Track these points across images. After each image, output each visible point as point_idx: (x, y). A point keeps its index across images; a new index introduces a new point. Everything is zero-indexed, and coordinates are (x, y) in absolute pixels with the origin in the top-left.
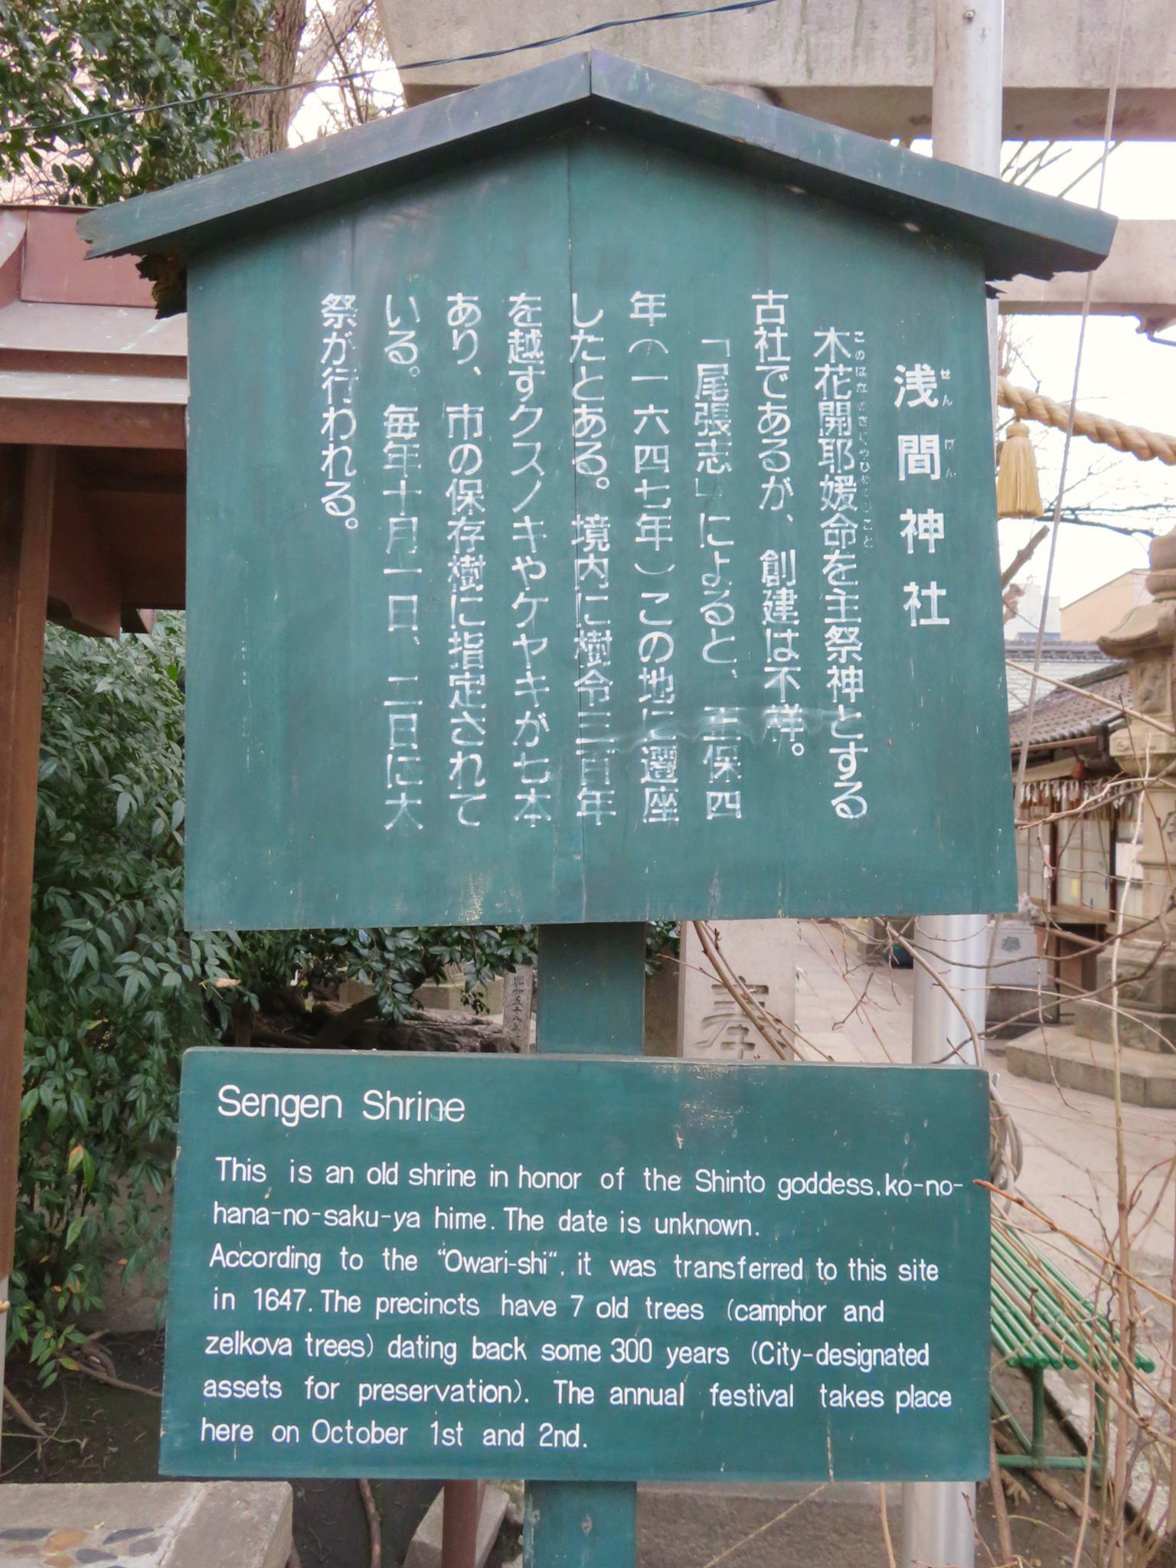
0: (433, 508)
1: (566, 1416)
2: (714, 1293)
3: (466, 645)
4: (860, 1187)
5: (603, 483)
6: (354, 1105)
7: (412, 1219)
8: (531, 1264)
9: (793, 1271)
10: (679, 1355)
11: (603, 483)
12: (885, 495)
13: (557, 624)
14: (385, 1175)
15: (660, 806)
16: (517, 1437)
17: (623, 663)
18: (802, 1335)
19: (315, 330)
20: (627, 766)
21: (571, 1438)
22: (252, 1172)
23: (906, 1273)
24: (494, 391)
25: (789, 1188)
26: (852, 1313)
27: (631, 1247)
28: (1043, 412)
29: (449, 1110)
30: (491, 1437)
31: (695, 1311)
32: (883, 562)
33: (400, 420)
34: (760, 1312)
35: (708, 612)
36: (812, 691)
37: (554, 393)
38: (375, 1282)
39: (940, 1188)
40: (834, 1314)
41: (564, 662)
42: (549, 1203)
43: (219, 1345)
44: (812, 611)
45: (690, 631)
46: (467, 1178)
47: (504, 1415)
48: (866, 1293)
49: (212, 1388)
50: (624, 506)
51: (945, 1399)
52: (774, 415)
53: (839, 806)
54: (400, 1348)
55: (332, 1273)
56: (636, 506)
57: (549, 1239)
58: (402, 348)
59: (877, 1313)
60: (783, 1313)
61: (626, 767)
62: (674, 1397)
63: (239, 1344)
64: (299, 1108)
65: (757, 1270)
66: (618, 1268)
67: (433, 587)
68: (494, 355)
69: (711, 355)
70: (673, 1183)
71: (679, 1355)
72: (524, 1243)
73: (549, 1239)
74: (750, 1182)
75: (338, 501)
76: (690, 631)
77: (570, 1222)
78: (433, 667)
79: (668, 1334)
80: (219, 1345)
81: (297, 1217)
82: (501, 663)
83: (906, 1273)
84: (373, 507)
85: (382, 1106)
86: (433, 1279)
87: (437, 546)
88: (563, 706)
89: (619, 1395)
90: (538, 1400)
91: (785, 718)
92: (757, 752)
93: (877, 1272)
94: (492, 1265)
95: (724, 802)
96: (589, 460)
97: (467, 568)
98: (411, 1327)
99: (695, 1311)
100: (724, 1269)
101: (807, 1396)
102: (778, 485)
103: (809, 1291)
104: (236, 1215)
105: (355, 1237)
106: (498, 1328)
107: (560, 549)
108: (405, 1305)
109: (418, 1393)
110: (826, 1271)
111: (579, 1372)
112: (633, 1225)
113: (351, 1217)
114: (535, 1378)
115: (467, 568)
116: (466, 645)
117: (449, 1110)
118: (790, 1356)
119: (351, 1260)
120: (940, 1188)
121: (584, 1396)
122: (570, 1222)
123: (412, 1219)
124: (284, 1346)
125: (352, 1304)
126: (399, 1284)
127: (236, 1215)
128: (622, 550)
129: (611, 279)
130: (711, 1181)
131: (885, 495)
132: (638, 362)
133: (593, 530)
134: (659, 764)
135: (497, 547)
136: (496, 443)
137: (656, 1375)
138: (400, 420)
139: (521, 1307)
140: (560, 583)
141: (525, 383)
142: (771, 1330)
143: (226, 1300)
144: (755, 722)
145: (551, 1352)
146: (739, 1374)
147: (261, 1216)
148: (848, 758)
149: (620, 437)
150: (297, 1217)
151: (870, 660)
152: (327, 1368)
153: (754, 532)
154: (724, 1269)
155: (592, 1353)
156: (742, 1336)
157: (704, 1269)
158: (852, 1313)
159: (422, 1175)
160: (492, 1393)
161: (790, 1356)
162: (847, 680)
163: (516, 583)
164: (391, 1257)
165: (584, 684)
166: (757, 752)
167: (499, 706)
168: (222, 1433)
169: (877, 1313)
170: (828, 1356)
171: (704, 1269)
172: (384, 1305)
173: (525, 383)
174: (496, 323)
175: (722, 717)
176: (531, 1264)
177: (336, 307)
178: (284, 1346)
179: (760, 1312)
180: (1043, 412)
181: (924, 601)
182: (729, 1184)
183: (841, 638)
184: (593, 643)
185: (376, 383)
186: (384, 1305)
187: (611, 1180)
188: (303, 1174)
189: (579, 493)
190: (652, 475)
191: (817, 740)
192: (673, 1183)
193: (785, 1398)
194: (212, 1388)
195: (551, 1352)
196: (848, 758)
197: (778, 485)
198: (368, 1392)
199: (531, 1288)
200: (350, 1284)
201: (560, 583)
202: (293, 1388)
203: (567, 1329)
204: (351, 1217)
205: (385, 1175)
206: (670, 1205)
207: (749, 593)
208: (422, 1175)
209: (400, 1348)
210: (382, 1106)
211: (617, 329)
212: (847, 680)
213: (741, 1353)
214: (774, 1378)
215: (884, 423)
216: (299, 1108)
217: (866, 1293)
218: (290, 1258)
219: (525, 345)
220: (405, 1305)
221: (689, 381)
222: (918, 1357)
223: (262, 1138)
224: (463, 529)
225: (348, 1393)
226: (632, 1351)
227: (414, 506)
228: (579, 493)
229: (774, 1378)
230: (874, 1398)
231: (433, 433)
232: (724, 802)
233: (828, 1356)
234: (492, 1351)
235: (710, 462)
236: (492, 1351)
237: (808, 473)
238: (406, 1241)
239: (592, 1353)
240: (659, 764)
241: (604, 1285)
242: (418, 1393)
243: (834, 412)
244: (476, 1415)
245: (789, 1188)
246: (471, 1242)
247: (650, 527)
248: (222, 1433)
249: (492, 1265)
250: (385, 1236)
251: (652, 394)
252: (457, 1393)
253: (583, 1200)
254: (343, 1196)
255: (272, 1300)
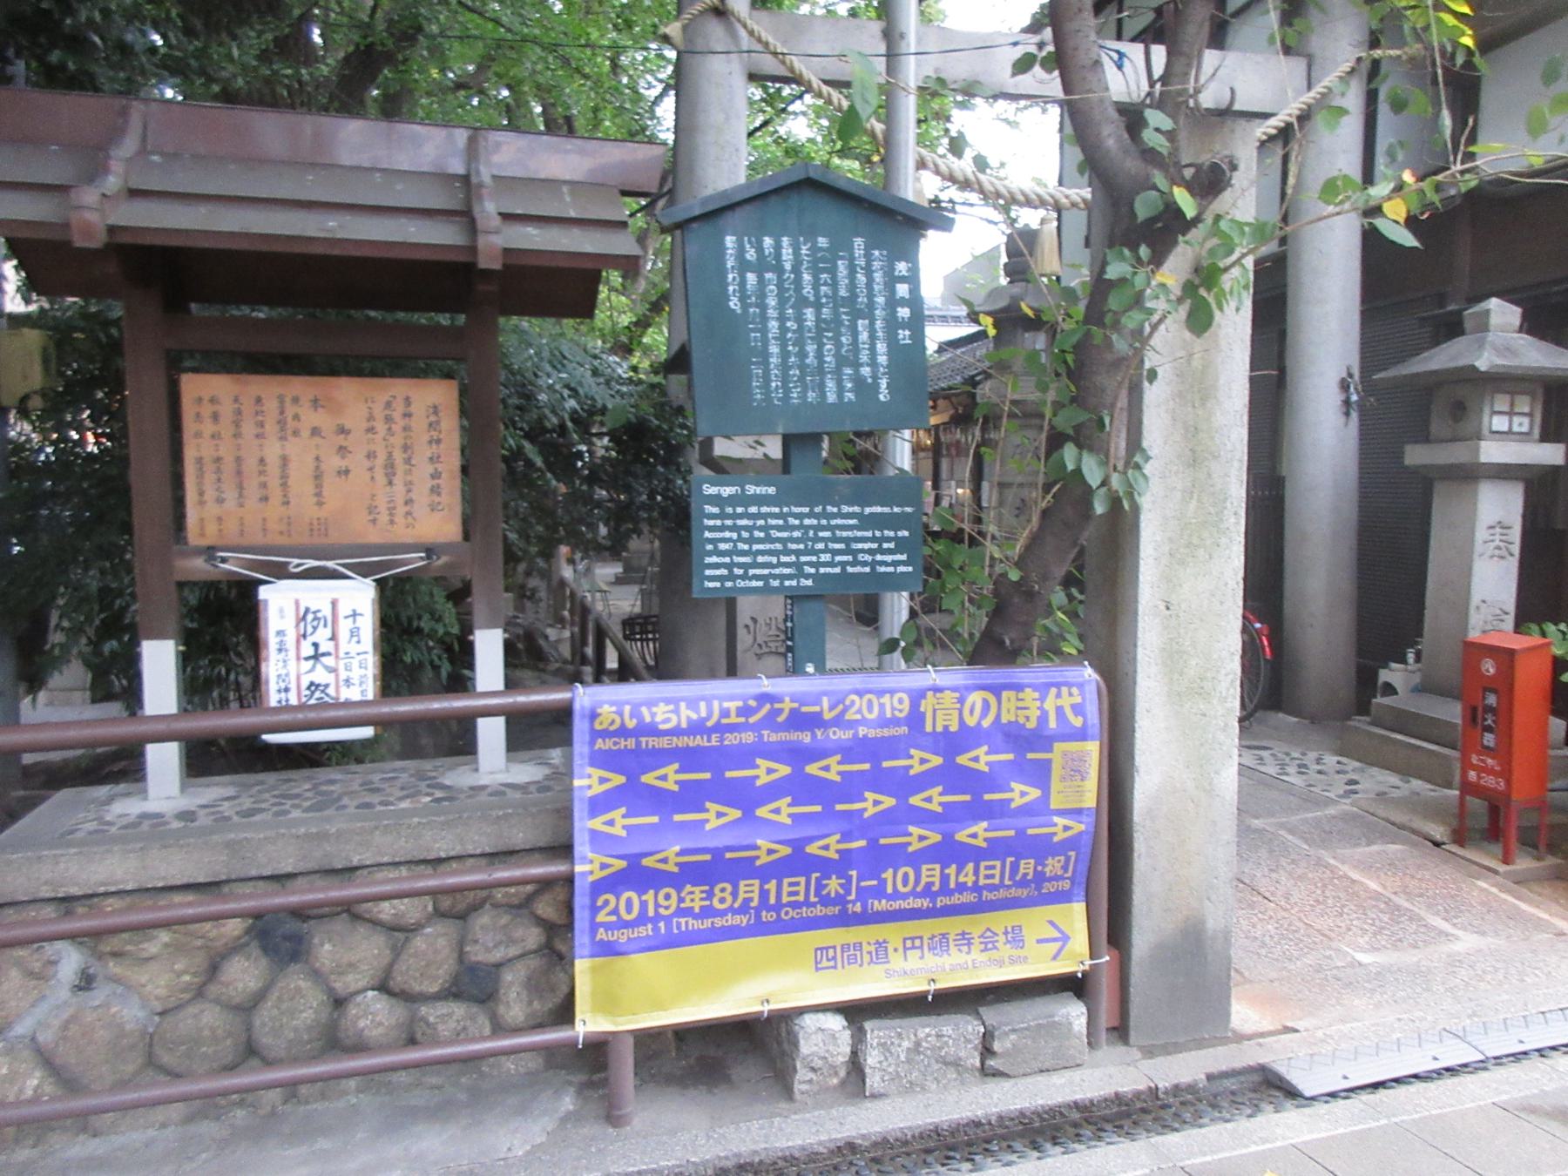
0: (763, 307)
1: (807, 577)
2: (847, 541)
3: (774, 349)
4: (886, 510)
5: (812, 299)
6: (743, 490)
7: (761, 522)
8: (796, 534)
9: (869, 534)
10: (838, 558)
11: (812, 299)
12: (893, 303)
13: (800, 342)
14: (753, 510)
15: (831, 397)
16: (794, 583)
17: (820, 355)
18: (871, 552)
19: (723, 248)
20: (822, 386)
21: (809, 583)
22: (715, 510)
23: (900, 534)
24: (779, 269)
25: (868, 510)
26: (885, 545)
27: (824, 528)
28: (1021, 198)
29: (771, 490)
30: (787, 583)
31: (842, 546)
32: (893, 324)
33: (751, 278)
34: (860, 546)
35: (844, 339)
36: (873, 363)
37: (796, 269)
38: (752, 540)
39: (909, 510)
40: (746, 572)
41: (802, 355)
42: (800, 516)
43: (708, 560)
44: (873, 337)
45: (838, 345)
46: (777, 510)
47: (789, 577)
48: (889, 540)
49: (708, 572)
50: (818, 306)
51: (911, 569)
52: (861, 278)
53: (881, 397)
54: (760, 559)
55: (740, 539)
56: (822, 305)
57: (801, 527)
58: (751, 255)
59: (892, 545)
60: (866, 546)
61: (821, 387)
62: (837, 570)
63: (714, 559)
64: (727, 491)
65: (859, 534)
66: (821, 534)
67: (764, 331)
68: (778, 255)
69: (842, 258)
70: (835, 510)
71: (838, 558)
72: (794, 528)
73: (801, 527)
74: (857, 509)
75: (734, 304)
76: (838, 345)
77: (807, 522)
78: (765, 355)
79: (835, 552)
80: (708, 560)
81: (729, 522)
82: (785, 354)
83: (900, 534)
84: (745, 306)
85: (752, 489)
86: (769, 539)
87: (764, 318)
88: (802, 367)
89: (822, 570)
90: (801, 574)
91: (866, 371)
92: (859, 381)
93: (892, 534)
94: (785, 535)
95: (849, 396)
96: (807, 290)
97: (773, 325)
98: (763, 553)
99: (842, 546)
100: (850, 534)
101: (873, 569)
102: (862, 299)
103: (873, 539)
104: (711, 523)
105: (746, 528)
106: (788, 552)
107: (800, 319)
108: (761, 547)
109: (766, 572)
110: (878, 534)
111: (810, 564)
112: (824, 522)
113: (744, 522)
114: (798, 566)
115: (773, 325)
116: (774, 349)
117: (771, 490)
118: (868, 558)
119: (745, 535)
120: (909, 510)
121: (813, 571)
122: (807, 522)
123: (761, 522)
124: (727, 560)
125: (746, 547)
126: (760, 541)
127: (711, 523)
128: (818, 320)
129: (811, 235)
130: (846, 509)
131: (893, 303)
132: (823, 260)
133: (809, 313)
134: (830, 385)
135: (782, 319)
136: (780, 285)
137: (831, 564)
138: (751, 278)
139: (794, 546)
140: (801, 328)
141: (788, 266)
142: (862, 551)
143: (710, 547)
144: (857, 371)
145: (803, 559)
146: (855, 563)
147: (719, 523)
148: (883, 383)
149: (816, 285)
150: (729, 522)
151: (890, 354)
152: (740, 565)
153: (856, 315)
154: (850, 534)
155: (814, 559)
156: (855, 553)
157: (845, 534)
158: (885, 545)
159: (764, 509)
160: (787, 571)
161: (868, 558)
162: (882, 359)
163: (788, 330)
164: (757, 534)
165: (808, 361)
166: (859, 381)
167: (785, 367)
168: (711, 585)
169: (892, 545)
170: (879, 557)
171: (845, 534)
172: (755, 547)
173: (788, 266)
174: (778, 247)
175: (848, 371)
176: (796, 534)
177: (730, 241)
178: (727, 560)
179: (860, 546)
180: (1021, 198)
181: (904, 335)
182: (851, 510)
183: (881, 347)
184: (811, 348)
185: (743, 266)
186: (755, 547)
187: (818, 509)
188: (729, 510)
189: (802, 302)
190: (826, 296)
191: (875, 377)
192: (835, 510)
193: (867, 569)
194: (708, 572)
195: (803, 559)
196: (883, 383)
197: (862, 299)
198: (752, 572)
199: (797, 541)
200: (745, 541)
201: (801, 328)
202: (731, 571)
203: (806, 552)
204: (744, 522)
205: (753, 510)
206: (834, 516)
207: (855, 333)
208: (764, 509)
209: (760, 559)
210: (752, 489)
211: (814, 249)
212: (882, 359)
213: (855, 558)
214: (865, 564)
215: (892, 280)
216: (727, 491)
217: (889, 540)
218: (727, 534)
219: (787, 253)
220: (761, 547)
221: (835, 266)
222: (904, 557)
223: (717, 500)
224: (772, 313)
225: (746, 572)
226: (825, 557)
227: (757, 306)
228: (802, 302)
229: (865, 564)
230: (891, 569)
231: (761, 282)
232: (849, 396)
233: (879, 557)
234: (784, 559)
235: (843, 293)
236: (784, 559)
237: (871, 296)
238: (760, 529)
239: (814, 559)
240: (830, 385)
241: (817, 539)
242: (766, 572)
243: (878, 276)
244: (783, 577)
245: (868, 510)
246: (779, 528)
247: (826, 312)
248: (711, 585)
249: (785, 535)
250: (754, 527)
251: (824, 270)
252: (777, 571)
253: (811, 515)
254: (741, 516)
255: (723, 546)
